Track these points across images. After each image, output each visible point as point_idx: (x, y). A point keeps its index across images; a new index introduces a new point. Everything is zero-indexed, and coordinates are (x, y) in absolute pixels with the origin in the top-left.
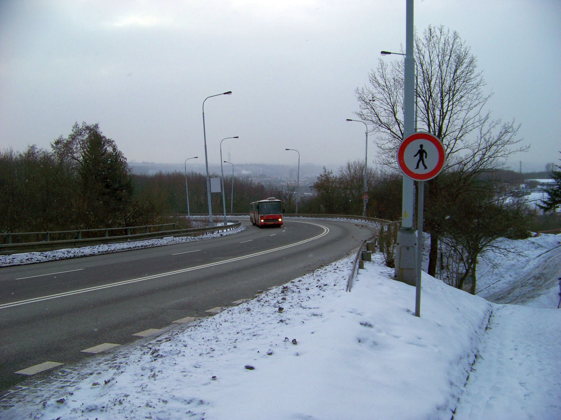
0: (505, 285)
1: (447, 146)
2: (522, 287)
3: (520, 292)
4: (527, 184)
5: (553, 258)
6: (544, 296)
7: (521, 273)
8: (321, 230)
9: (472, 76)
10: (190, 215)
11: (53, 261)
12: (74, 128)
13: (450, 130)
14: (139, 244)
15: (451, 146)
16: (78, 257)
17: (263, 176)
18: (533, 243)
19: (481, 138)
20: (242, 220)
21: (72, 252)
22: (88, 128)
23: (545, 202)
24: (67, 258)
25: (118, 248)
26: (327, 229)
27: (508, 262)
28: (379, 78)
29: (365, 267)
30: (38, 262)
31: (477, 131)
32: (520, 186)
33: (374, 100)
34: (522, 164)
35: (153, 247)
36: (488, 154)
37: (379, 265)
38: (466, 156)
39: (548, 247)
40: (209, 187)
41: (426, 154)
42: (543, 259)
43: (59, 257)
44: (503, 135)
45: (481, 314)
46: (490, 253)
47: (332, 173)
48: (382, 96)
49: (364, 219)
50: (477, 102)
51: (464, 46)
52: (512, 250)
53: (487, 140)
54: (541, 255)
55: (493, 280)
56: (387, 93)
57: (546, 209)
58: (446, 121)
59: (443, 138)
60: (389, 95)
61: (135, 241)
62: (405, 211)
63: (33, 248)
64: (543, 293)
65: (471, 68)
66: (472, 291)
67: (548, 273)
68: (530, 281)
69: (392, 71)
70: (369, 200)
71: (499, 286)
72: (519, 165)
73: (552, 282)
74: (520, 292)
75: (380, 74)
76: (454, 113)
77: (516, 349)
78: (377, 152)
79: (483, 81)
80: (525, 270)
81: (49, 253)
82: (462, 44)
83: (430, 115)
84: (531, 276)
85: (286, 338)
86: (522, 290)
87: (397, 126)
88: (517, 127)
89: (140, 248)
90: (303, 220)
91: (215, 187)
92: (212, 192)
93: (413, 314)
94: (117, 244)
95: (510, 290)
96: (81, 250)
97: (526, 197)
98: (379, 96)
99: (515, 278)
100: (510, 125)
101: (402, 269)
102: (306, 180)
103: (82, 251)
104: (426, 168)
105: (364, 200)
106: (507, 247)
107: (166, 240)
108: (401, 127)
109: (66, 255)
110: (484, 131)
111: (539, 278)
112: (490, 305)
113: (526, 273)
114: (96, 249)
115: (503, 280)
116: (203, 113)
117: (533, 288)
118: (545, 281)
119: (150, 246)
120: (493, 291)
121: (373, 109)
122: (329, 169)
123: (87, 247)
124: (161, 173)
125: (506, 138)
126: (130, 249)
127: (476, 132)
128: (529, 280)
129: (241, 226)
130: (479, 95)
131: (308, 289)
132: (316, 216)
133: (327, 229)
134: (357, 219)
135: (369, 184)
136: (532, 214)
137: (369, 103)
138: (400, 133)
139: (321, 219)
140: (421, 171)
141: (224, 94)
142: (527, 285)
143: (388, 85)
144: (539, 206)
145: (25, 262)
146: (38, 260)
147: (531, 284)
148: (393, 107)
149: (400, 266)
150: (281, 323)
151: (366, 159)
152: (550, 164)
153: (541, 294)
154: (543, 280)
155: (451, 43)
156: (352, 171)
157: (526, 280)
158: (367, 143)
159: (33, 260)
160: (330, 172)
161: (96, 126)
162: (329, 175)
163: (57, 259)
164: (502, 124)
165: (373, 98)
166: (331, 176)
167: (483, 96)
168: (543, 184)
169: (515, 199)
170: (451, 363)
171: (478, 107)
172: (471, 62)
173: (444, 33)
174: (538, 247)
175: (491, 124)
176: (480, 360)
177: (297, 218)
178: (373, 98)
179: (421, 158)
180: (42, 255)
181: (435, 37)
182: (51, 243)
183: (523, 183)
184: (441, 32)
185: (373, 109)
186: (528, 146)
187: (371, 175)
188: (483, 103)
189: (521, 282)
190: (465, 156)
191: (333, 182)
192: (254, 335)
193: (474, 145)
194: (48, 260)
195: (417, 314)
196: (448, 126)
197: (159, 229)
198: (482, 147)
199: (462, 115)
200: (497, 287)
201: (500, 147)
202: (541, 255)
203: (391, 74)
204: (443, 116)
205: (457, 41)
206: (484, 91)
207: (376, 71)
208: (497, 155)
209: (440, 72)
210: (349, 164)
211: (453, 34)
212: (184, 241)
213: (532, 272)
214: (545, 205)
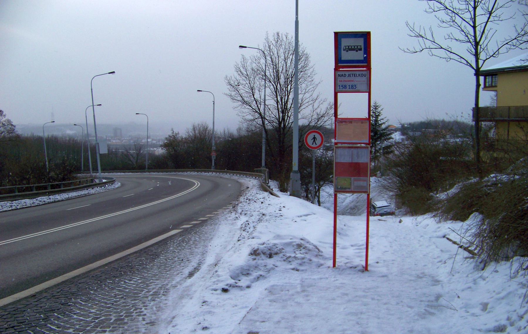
10: (93, 173)
11: (38, 206)
16: (56, 202)
28: (242, 69)
31: (310, 107)
33: (239, 85)
35: (89, 195)
47: (178, 134)
49: (214, 171)
68: (348, 211)
69: (251, 63)
70: (216, 157)
73: (363, 210)
81: (51, 197)
90: (155, 175)
92: (101, 153)
102: (130, 138)
104: (316, 144)
105: (213, 156)
110: (316, 106)
111: (354, 208)
122: (176, 131)
127: (310, 107)
128: (347, 210)
130: (313, 82)
135: (216, 144)
137: (235, 87)
147: (349, 212)
156: (197, 132)
157: (345, 211)
158: (214, 109)
160: (177, 132)
162: (176, 135)
163: (47, 203)
167: (315, 83)
175: (320, 102)
177: (148, 173)
179: (314, 141)
193: (308, 116)
207: (240, 64)
210: (194, 126)
213: (349, 205)
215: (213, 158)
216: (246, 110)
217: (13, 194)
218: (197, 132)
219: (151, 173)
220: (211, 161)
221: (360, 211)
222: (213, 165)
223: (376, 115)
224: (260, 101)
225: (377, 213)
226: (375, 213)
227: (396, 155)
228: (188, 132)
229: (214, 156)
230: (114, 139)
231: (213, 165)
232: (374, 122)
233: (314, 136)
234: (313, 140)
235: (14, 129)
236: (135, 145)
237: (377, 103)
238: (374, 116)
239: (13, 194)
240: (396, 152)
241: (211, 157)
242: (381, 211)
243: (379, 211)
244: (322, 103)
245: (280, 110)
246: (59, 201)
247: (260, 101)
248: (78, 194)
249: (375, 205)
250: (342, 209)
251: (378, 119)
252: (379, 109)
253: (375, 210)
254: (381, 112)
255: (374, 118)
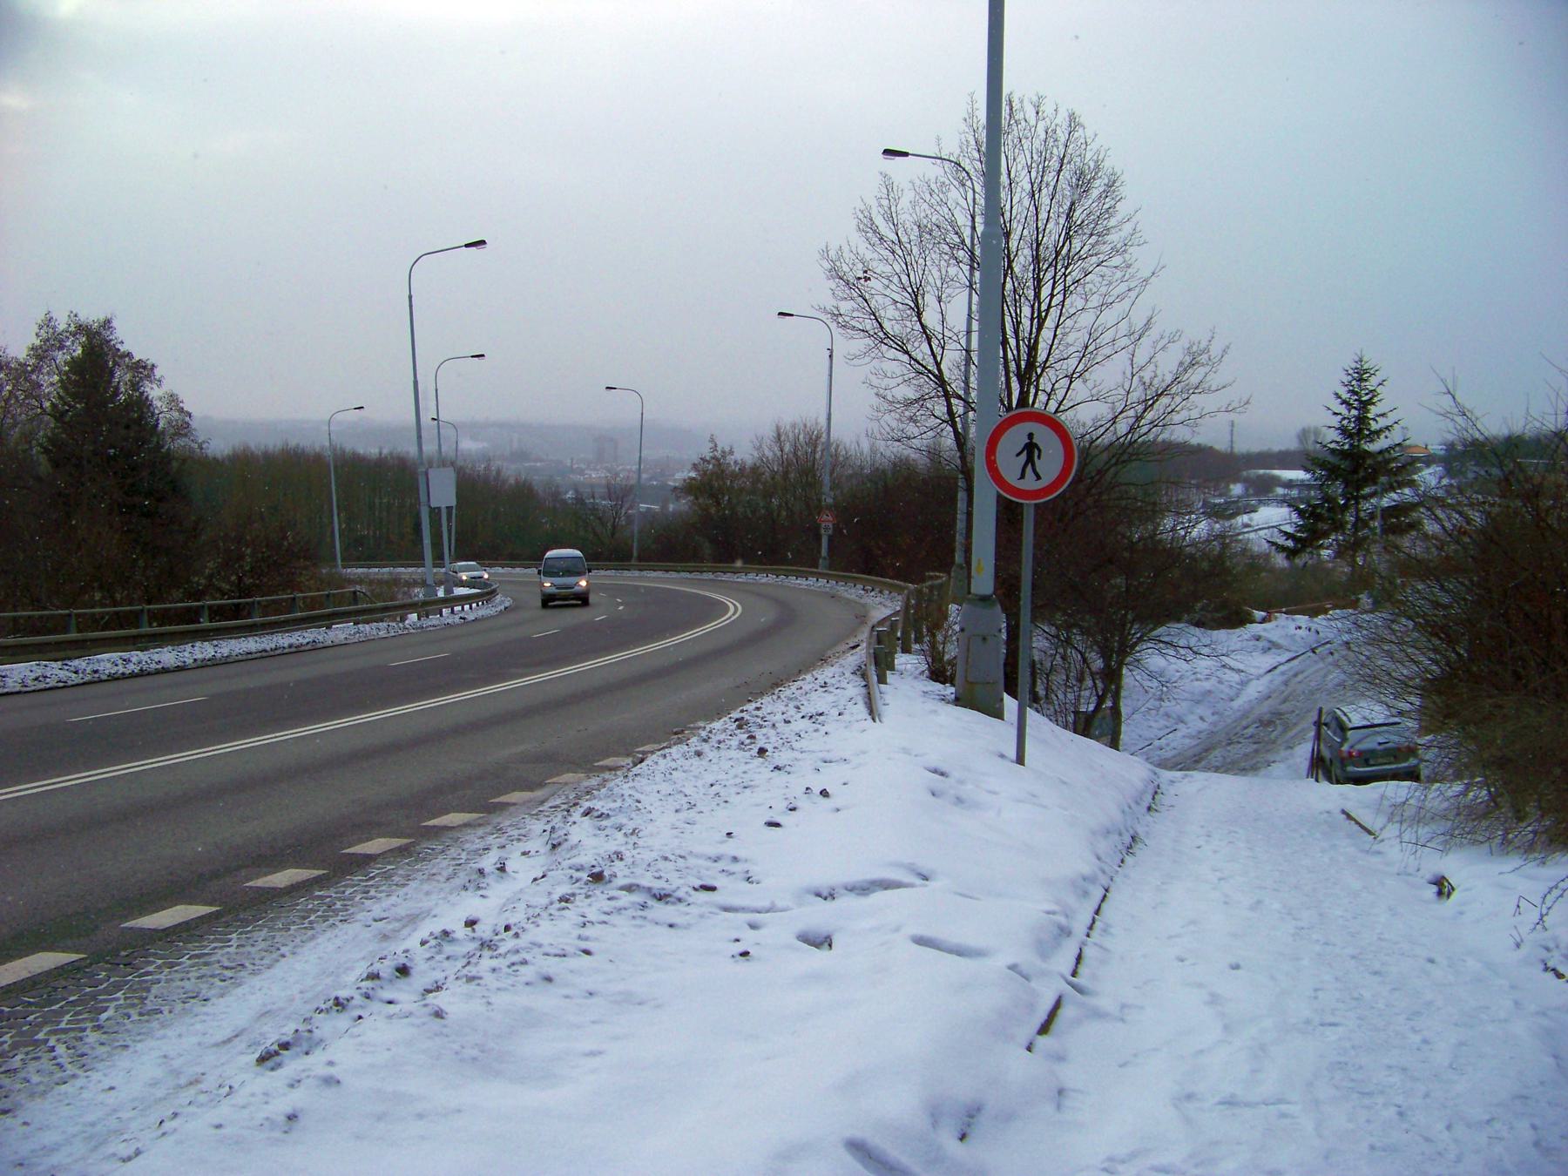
0: (1187, 741)
1: (1049, 395)
2: (1229, 744)
3: (1224, 758)
4: (1247, 482)
5: (1305, 674)
6: (1282, 766)
7: (1227, 713)
8: (714, 609)
9: (1113, 222)
11: (94, 682)
12: (41, 328)
13: (1056, 354)
14: (283, 640)
15: (1060, 394)
16: (149, 674)
17: (521, 455)
18: (1258, 638)
19: (1133, 376)
20: (500, 582)
21: (134, 659)
22: (81, 329)
23: (1288, 536)
24: (124, 677)
25: (237, 651)
26: (734, 605)
27: (1197, 683)
29: (888, 681)
30: (61, 684)
31: (1122, 359)
32: (1230, 490)
33: (869, 279)
34: (1235, 429)
35: (315, 647)
36: (1149, 416)
37: (916, 678)
38: (1095, 420)
39: (1293, 648)
40: (425, 489)
41: (1040, 451)
42: (1280, 679)
43: (107, 672)
44: (1186, 370)
45: (1140, 785)
46: (1154, 659)
47: (731, 452)
48: (888, 269)
50: (1123, 287)
51: (1093, 146)
52: (1206, 651)
53: (1148, 382)
54: (1275, 668)
55: (1160, 729)
56: (900, 260)
57: (1291, 553)
58: (1047, 334)
59: (1039, 377)
60: (906, 264)
61: (272, 634)
62: (979, 560)
63: (40, 652)
64: (1278, 758)
65: (1109, 202)
66: (1114, 743)
67: (1293, 711)
68: (1250, 731)
69: (914, 204)
71: (1173, 745)
72: (1228, 429)
74: (1224, 758)
75: (882, 212)
76: (1067, 315)
77: (1209, 836)
78: (872, 407)
79: (1138, 235)
80: (1236, 704)
82: (1089, 141)
83: (1008, 319)
84: (1252, 717)
85: (807, 789)
86: (1229, 751)
87: (925, 347)
88: (1220, 353)
89: (286, 651)
90: (634, 578)
91: (227, 463)
93: (1012, 762)
94: (233, 641)
95: (1200, 753)
96: (153, 658)
97: (1245, 518)
98: (881, 268)
99: (1214, 724)
100: (1202, 346)
101: (972, 683)
103: (156, 657)
104: (1038, 478)
105: (823, 525)
106: (1193, 642)
107: (341, 632)
108: (934, 346)
109: (121, 669)
110: (1140, 359)
111: (1270, 723)
112: (1155, 774)
113: (1239, 710)
114: (186, 654)
115: (1183, 730)
116: (410, 297)
117: (1255, 746)
118: (1285, 731)
119: (309, 647)
120: (1159, 756)
121: (866, 301)
122: (723, 444)
123: (165, 649)
124: (246, 449)
125: (1194, 377)
126: (264, 654)
127: (1122, 359)
128: (1245, 728)
129: (499, 598)
130: (1130, 270)
131: (789, 722)
132: (691, 569)
133: (734, 605)
134: (806, 576)
135: (835, 485)
136: (1256, 564)
137: (855, 284)
138: (932, 361)
139: (706, 576)
140: (1030, 484)
141: (467, 246)
142: (1241, 740)
143: (904, 239)
144: (1273, 544)
145: (32, 686)
146: (60, 681)
147: (1251, 737)
148: (916, 296)
149: (966, 677)
150: (777, 772)
151: (829, 419)
152: (1309, 428)
153: (1274, 762)
154: (1280, 728)
155: (1063, 139)
156: (787, 448)
158: (831, 376)
159: (48, 680)
160: (727, 449)
161: (107, 323)
164: (1183, 343)
165: (865, 272)
166: (730, 459)
167: (1139, 275)
168: (1289, 484)
169: (1216, 522)
170: (1094, 833)
171: (1126, 303)
172: (1111, 185)
173: (1045, 115)
174: (1269, 649)
176: (1140, 845)
177: (637, 573)
178: (865, 272)
179: (1030, 460)
180: (66, 668)
181: (1023, 123)
182: (81, 638)
183: (1235, 481)
184: (1037, 113)
185: (866, 301)
186: (1245, 399)
187: (838, 461)
188: (1137, 289)
189: (1227, 734)
190: (1093, 420)
191: (734, 476)
192: (745, 787)
194: (82, 681)
195: (1020, 760)
196: (1051, 346)
197: (313, 604)
198: (1134, 397)
199: (1086, 319)
200: (1168, 745)
201: (1178, 399)
202: (1275, 668)
203: (911, 211)
204: (1038, 321)
205: (1076, 135)
206: (1142, 260)
207: (874, 204)
208: (1171, 419)
209: (1032, 208)
210: (778, 428)
211: (1067, 119)
212: (382, 634)
214: (1290, 543)
215: (823, 531)
216: (893, 364)
217: (134, 631)
218: (787, 448)
219: (645, 573)
220: (818, 538)
221: (1291, 733)
222: (824, 552)
223: (1361, 402)
224: (940, 336)
225: (1352, 747)
226: (1343, 749)
227: (1426, 536)
228: (759, 448)
229: (827, 522)
230: (595, 469)
231: (824, 552)
232: (1353, 425)
233: (1030, 436)
234: (1024, 456)
235: (188, 423)
236: (608, 486)
237: (1365, 359)
238: (1356, 404)
239: (134, 631)
240: (1431, 527)
241: (818, 528)
242: (1368, 740)
243: (1360, 741)
244: (1163, 348)
245: (1011, 369)
246: (165, 671)
247: (940, 336)
248: (260, 647)
249: (1344, 718)
250: (1229, 721)
251: (1369, 415)
252: (1372, 383)
253: (1344, 739)
254: (1379, 390)
255: (1354, 412)
